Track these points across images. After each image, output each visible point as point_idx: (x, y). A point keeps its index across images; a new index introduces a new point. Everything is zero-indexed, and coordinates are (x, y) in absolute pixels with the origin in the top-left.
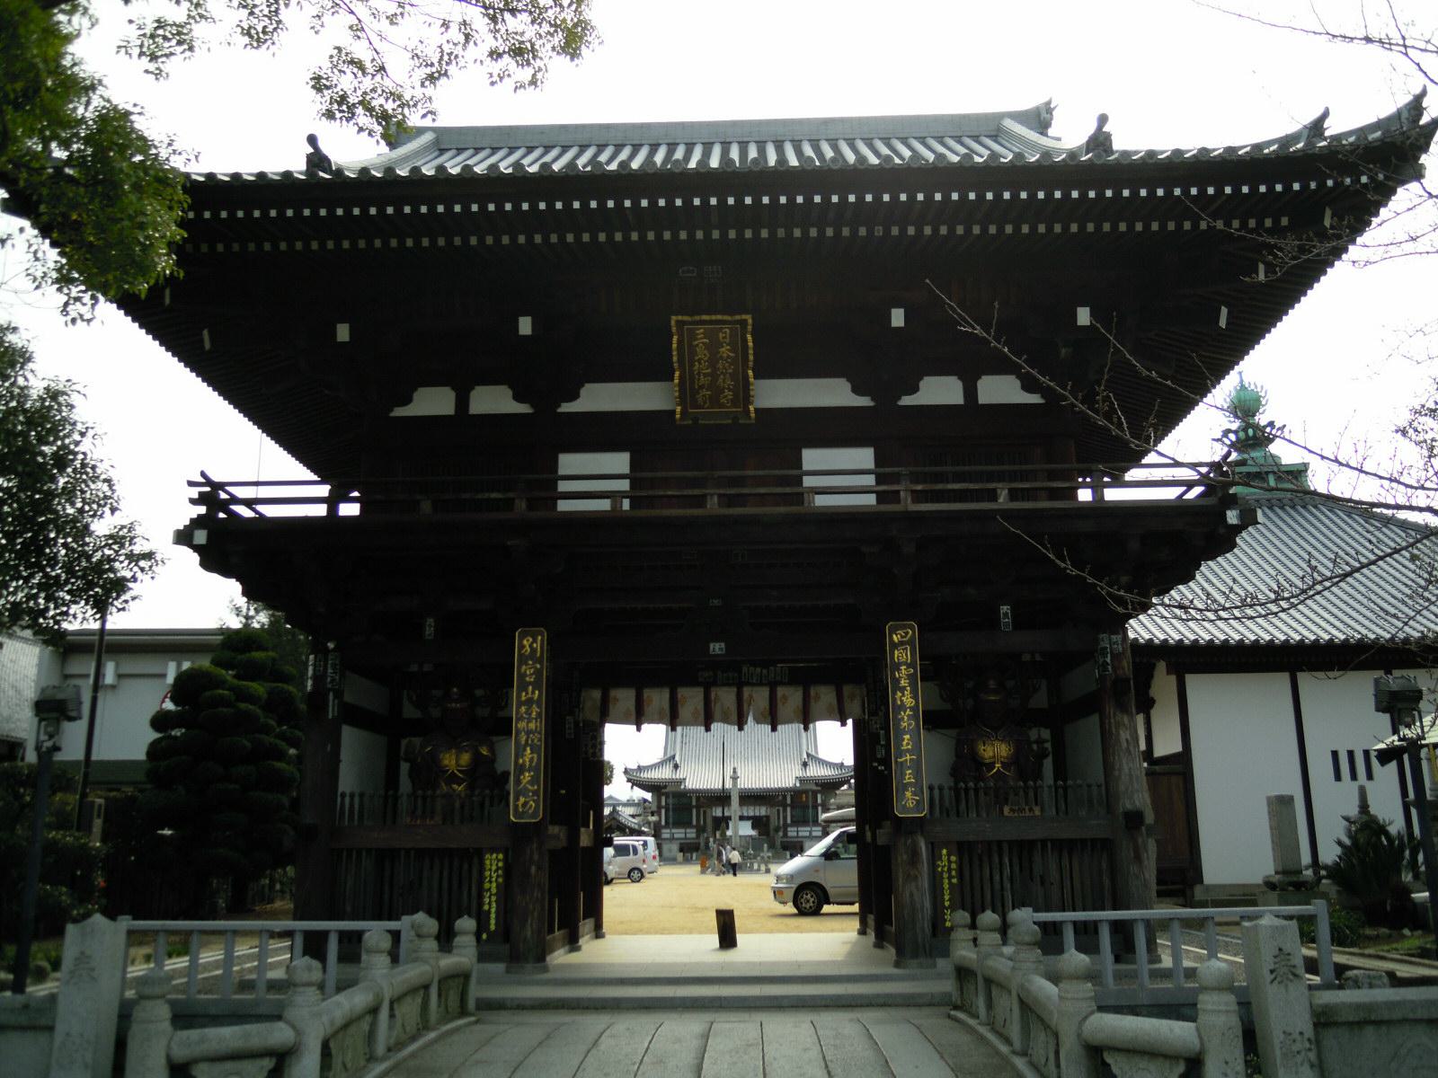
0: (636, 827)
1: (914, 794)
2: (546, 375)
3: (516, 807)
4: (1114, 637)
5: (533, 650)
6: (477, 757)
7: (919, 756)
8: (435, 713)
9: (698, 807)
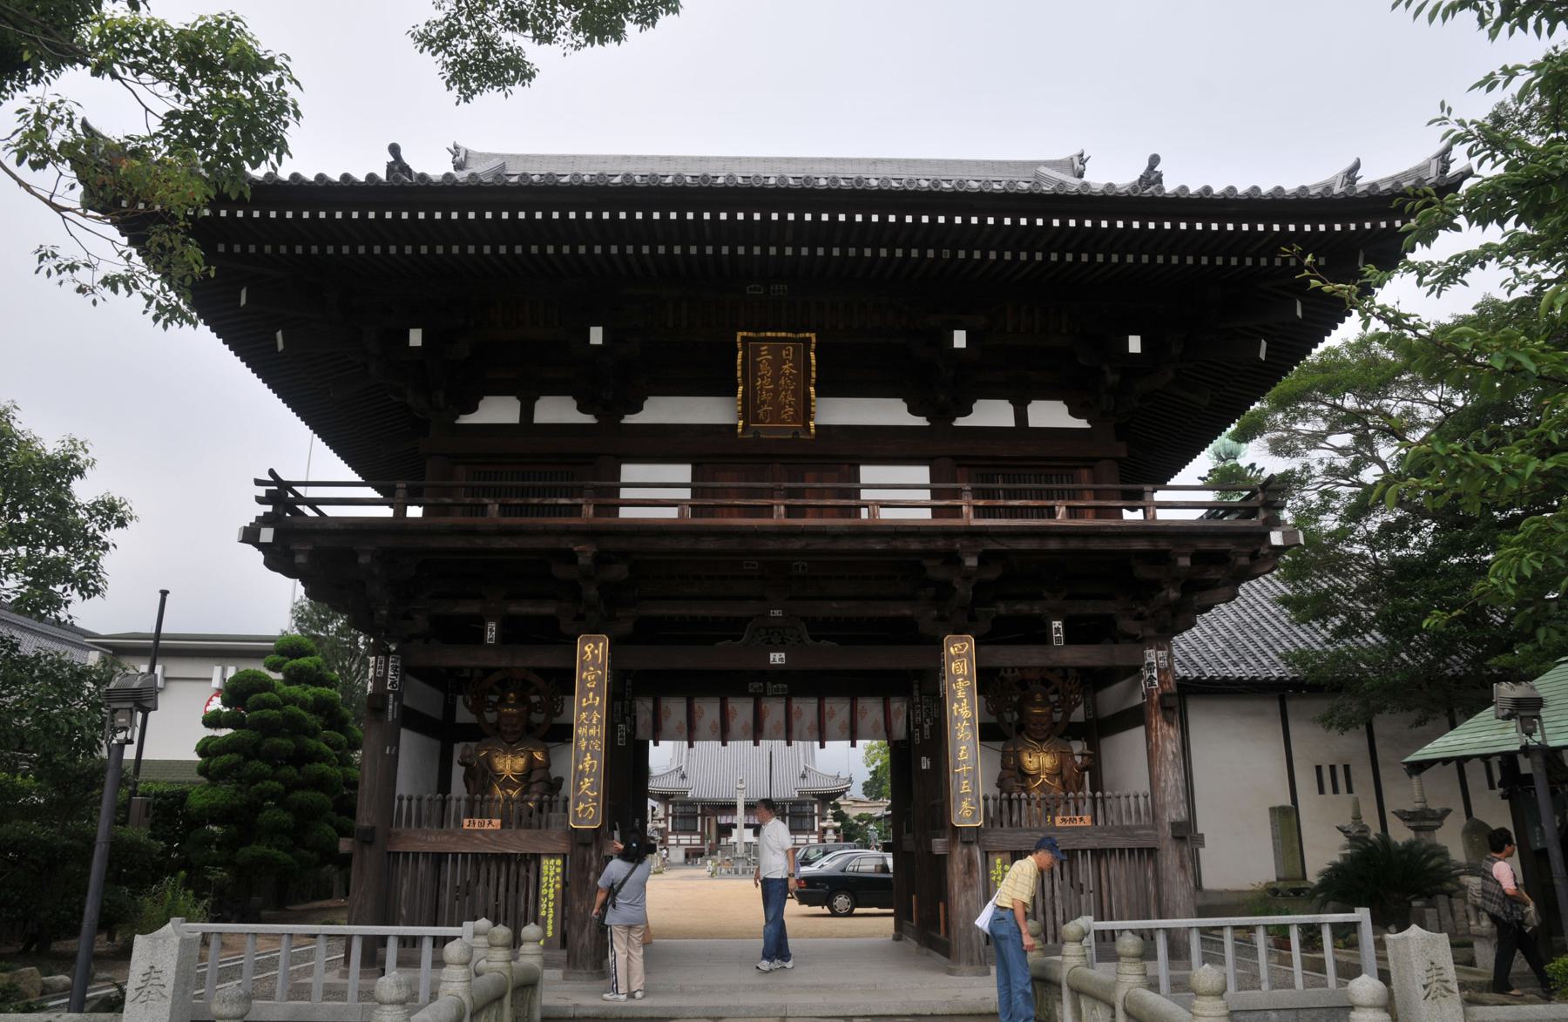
2: (611, 387)
4: (1160, 653)
5: (595, 657)
7: (976, 768)
8: (491, 717)
9: (703, 816)
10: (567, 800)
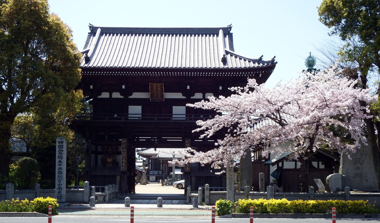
1: (188, 168)
6: (113, 159)
9: (163, 164)
10: (120, 166)
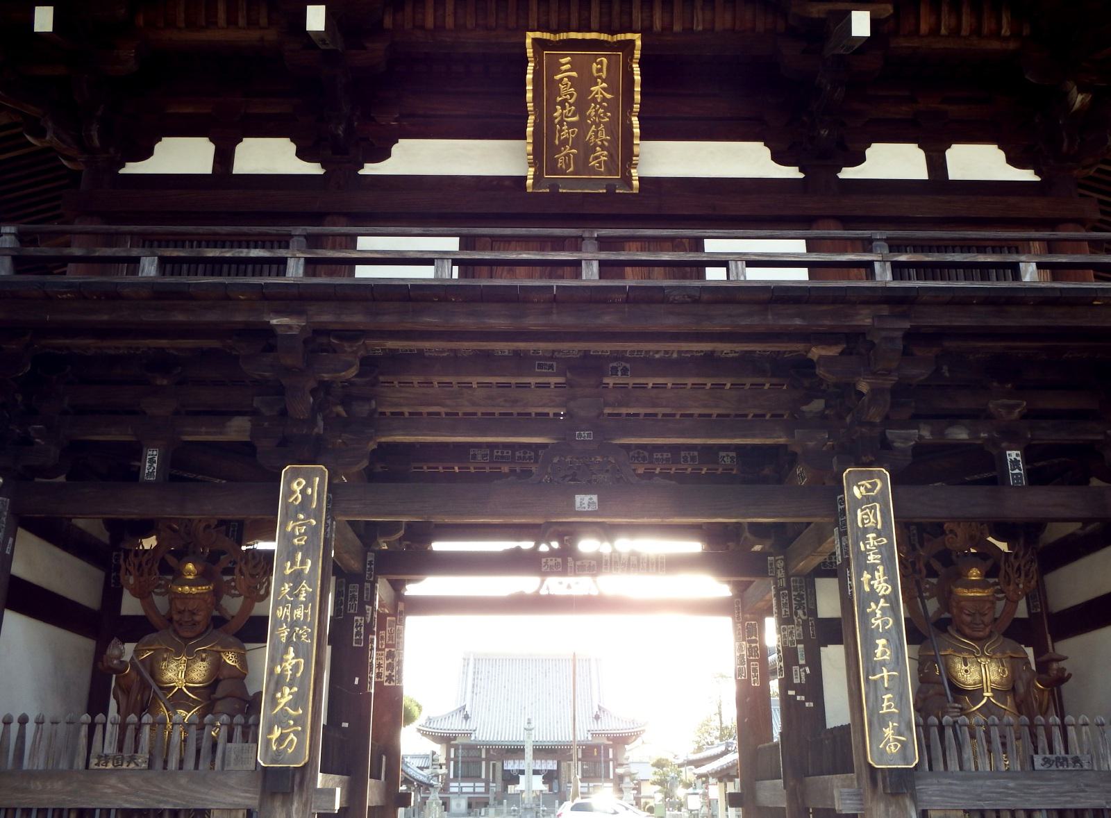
0: (425, 780)
3: (268, 742)
6: (218, 666)
9: (488, 760)
